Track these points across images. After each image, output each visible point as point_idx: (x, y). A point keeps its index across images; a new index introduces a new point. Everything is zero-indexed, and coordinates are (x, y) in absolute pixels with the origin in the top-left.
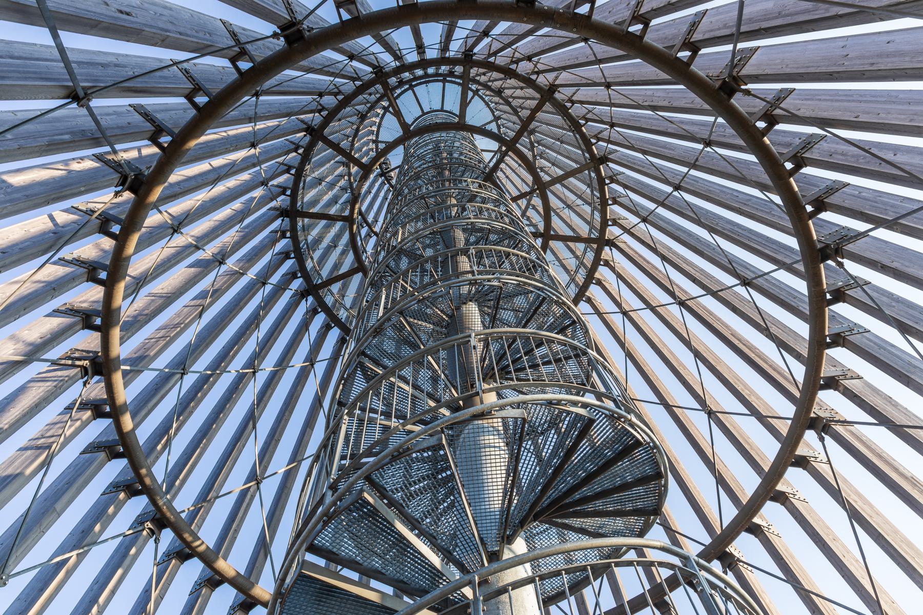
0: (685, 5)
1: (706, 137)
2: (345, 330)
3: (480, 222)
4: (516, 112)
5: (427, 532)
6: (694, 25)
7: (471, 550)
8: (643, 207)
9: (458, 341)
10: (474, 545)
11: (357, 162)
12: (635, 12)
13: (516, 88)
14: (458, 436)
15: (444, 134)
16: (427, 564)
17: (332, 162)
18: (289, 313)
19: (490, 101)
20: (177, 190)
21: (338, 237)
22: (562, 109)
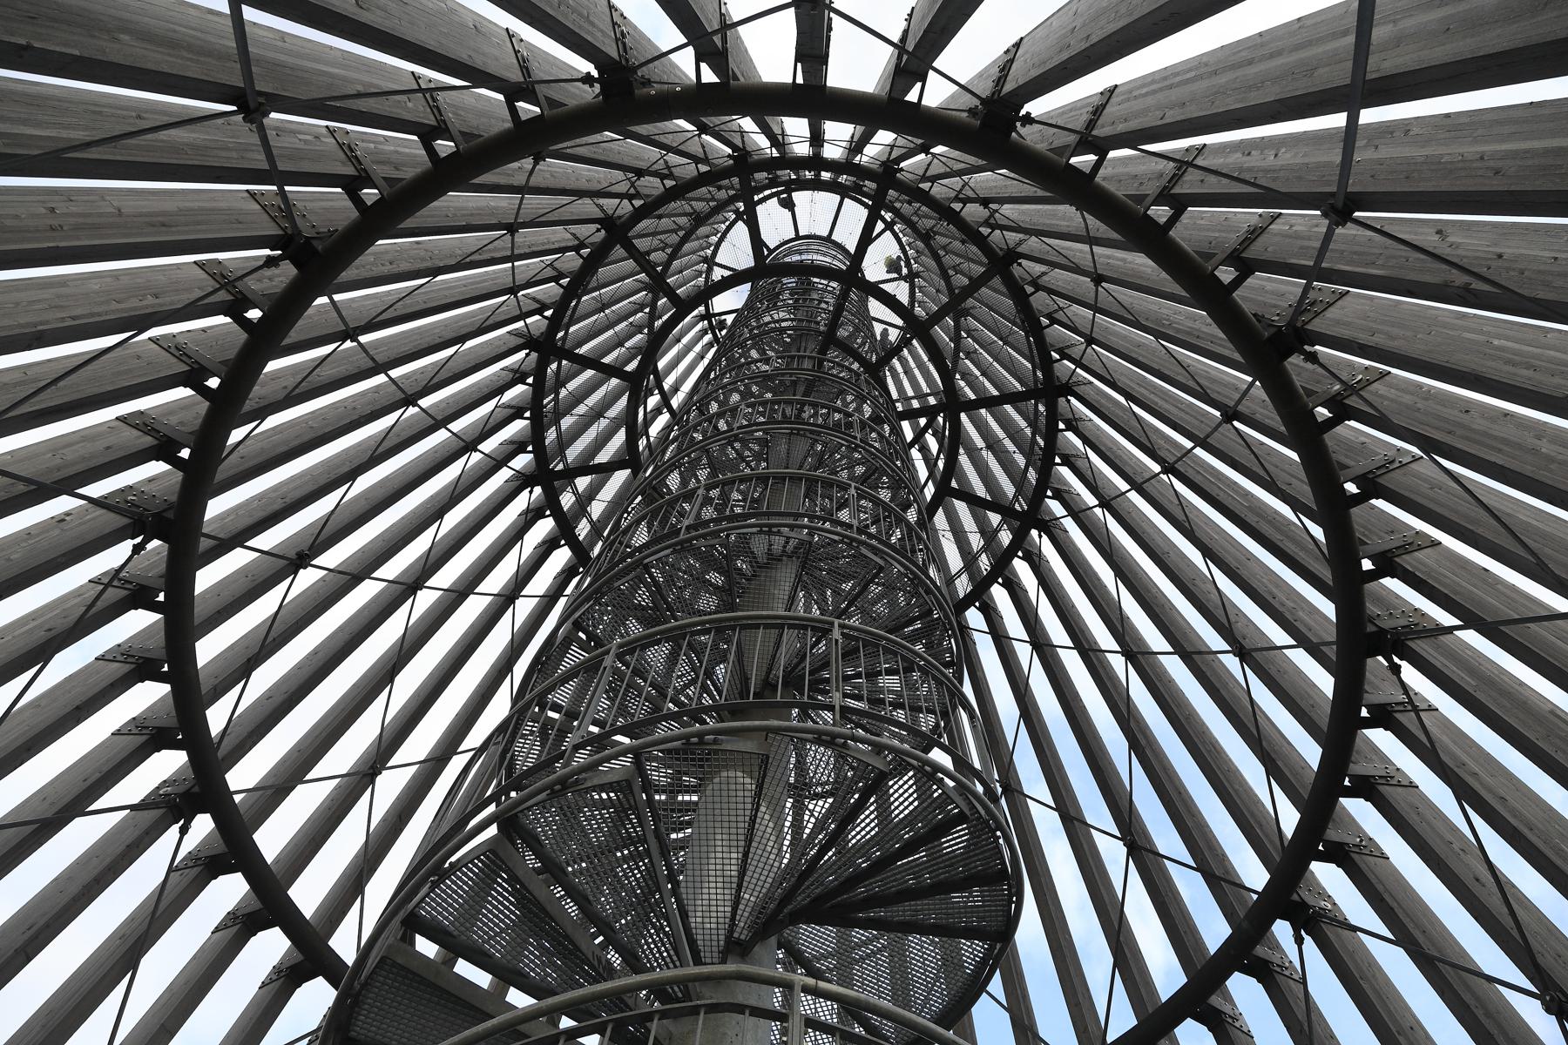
2: (580, 551)
6: (1255, 233)
11: (670, 293)
13: (955, 238)
19: (909, 245)
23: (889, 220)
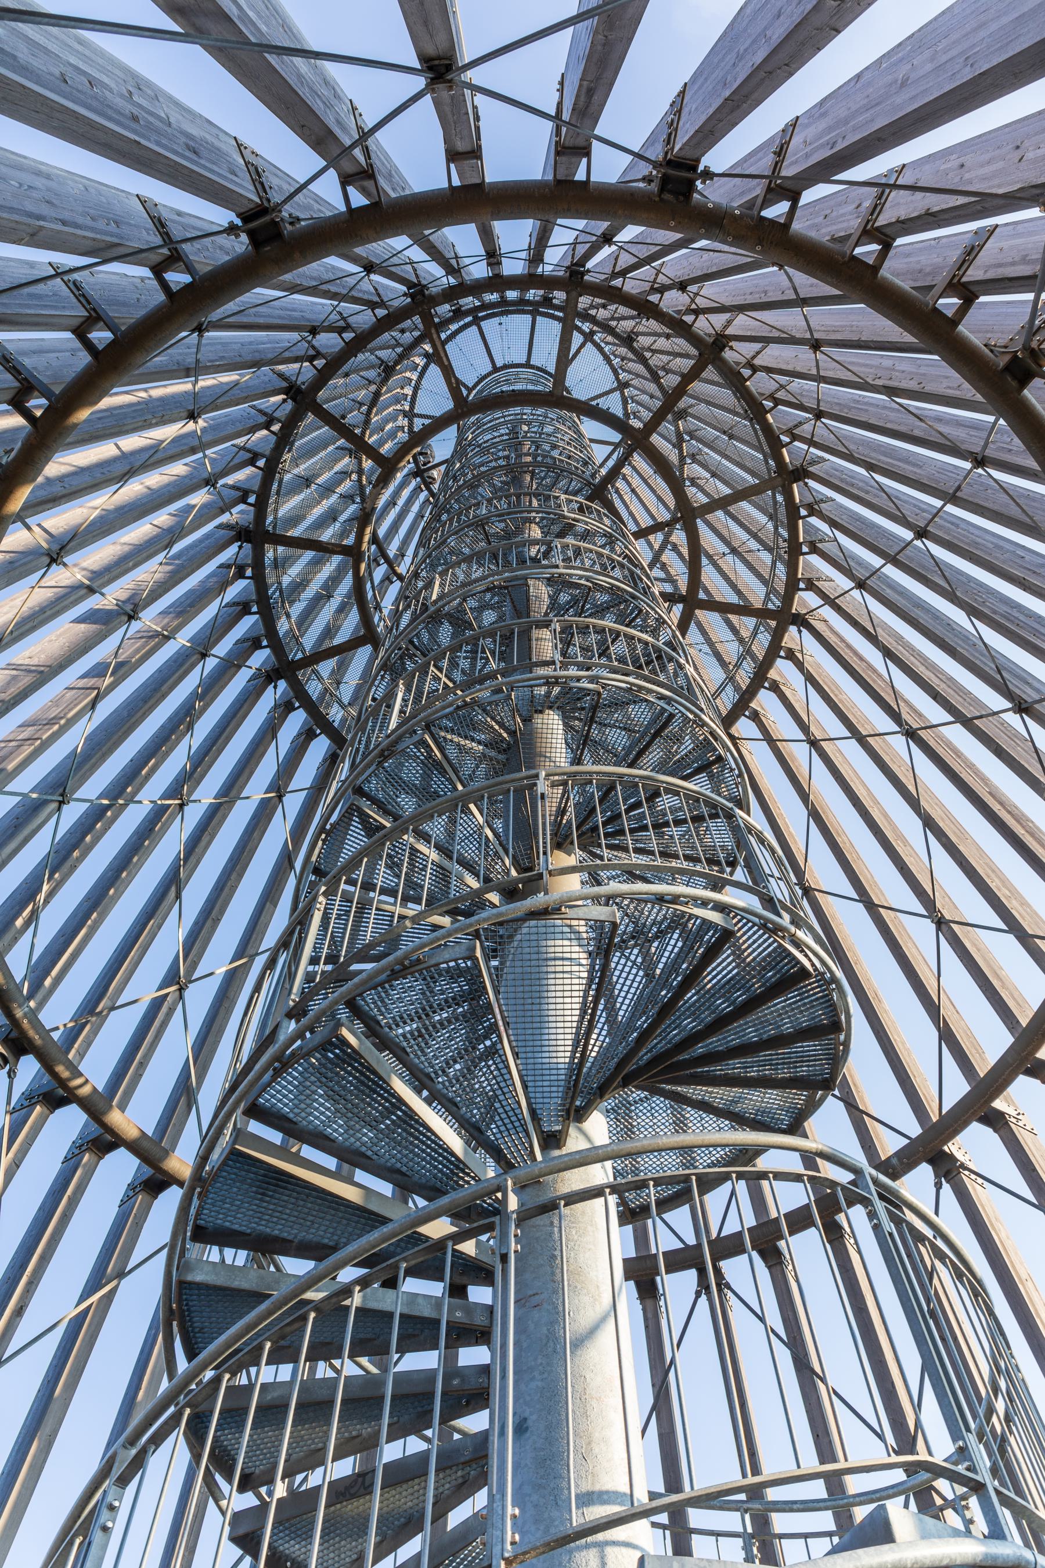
0: (955, 217)
1: (977, 449)
2: (338, 739)
3: (576, 574)
4: (655, 378)
5: (445, 1096)
6: (971, 253)
7: (515, 1128)
8: (861, 562)
9: (517, 784)
10: (519, 1120)
11: (372, 452)
12: (868, 221)
13: (659, 335)
14: (511, 937)
15: (527, 410)
16: (440, 1146)
17: (331, 448)
18: (245, 707)
19: (613, 354)
20: (57, 489)
21: (334, 580)
22: (734, 379)
23: (588, 331)
